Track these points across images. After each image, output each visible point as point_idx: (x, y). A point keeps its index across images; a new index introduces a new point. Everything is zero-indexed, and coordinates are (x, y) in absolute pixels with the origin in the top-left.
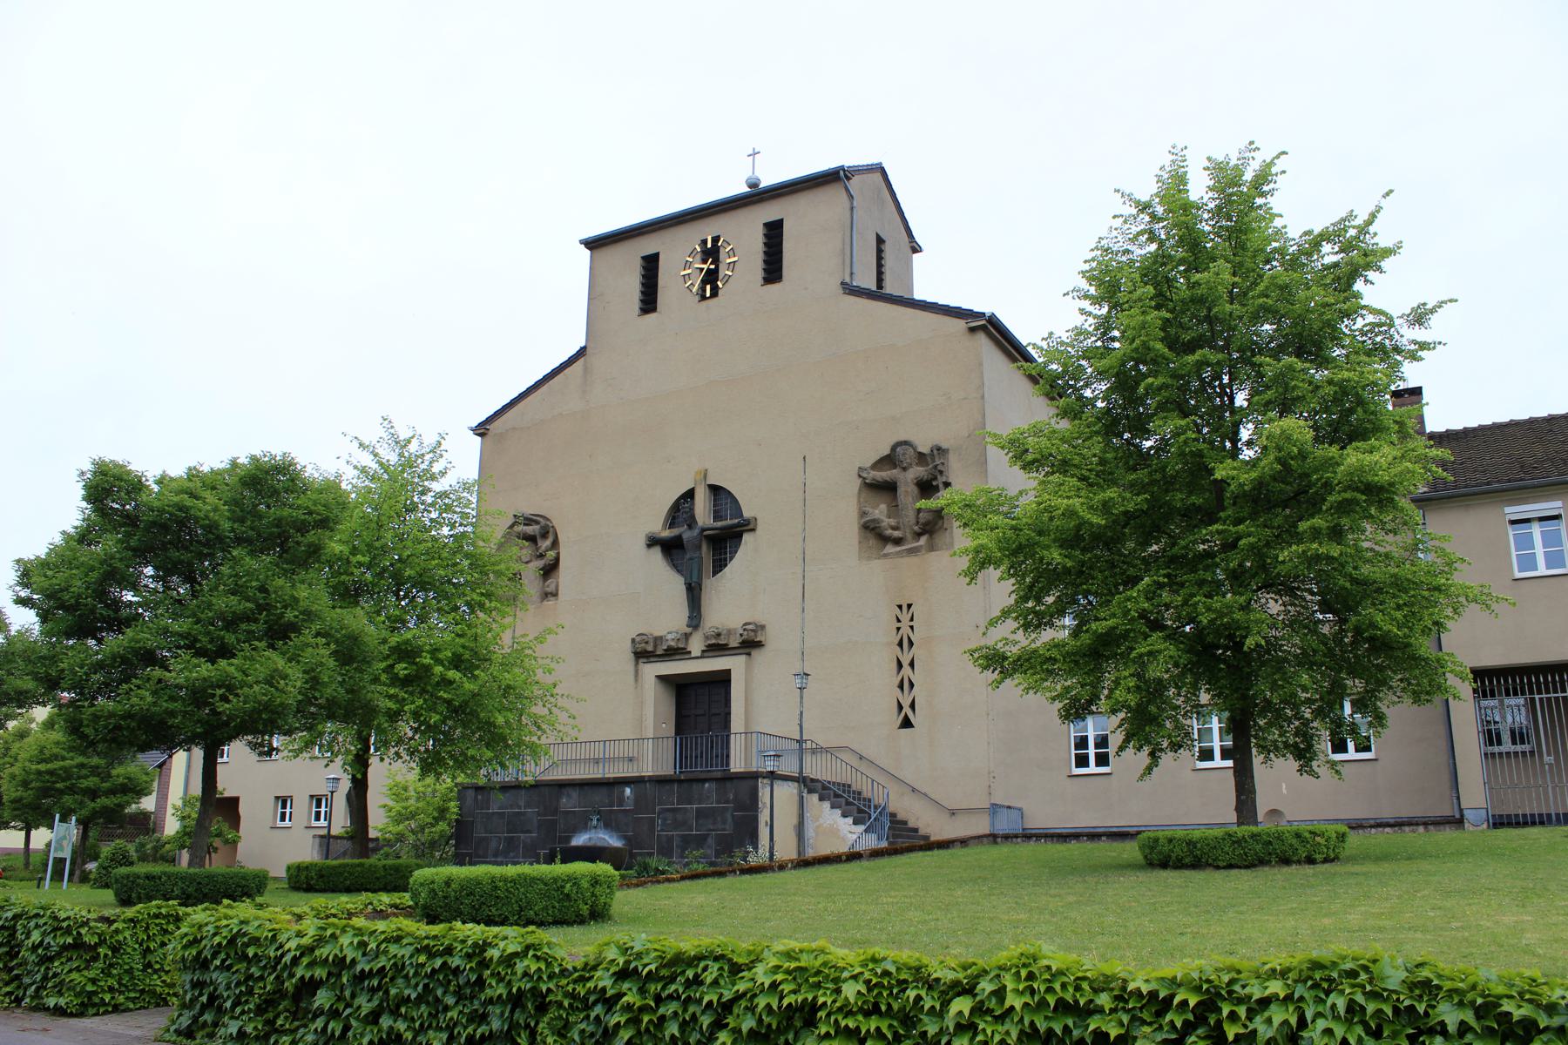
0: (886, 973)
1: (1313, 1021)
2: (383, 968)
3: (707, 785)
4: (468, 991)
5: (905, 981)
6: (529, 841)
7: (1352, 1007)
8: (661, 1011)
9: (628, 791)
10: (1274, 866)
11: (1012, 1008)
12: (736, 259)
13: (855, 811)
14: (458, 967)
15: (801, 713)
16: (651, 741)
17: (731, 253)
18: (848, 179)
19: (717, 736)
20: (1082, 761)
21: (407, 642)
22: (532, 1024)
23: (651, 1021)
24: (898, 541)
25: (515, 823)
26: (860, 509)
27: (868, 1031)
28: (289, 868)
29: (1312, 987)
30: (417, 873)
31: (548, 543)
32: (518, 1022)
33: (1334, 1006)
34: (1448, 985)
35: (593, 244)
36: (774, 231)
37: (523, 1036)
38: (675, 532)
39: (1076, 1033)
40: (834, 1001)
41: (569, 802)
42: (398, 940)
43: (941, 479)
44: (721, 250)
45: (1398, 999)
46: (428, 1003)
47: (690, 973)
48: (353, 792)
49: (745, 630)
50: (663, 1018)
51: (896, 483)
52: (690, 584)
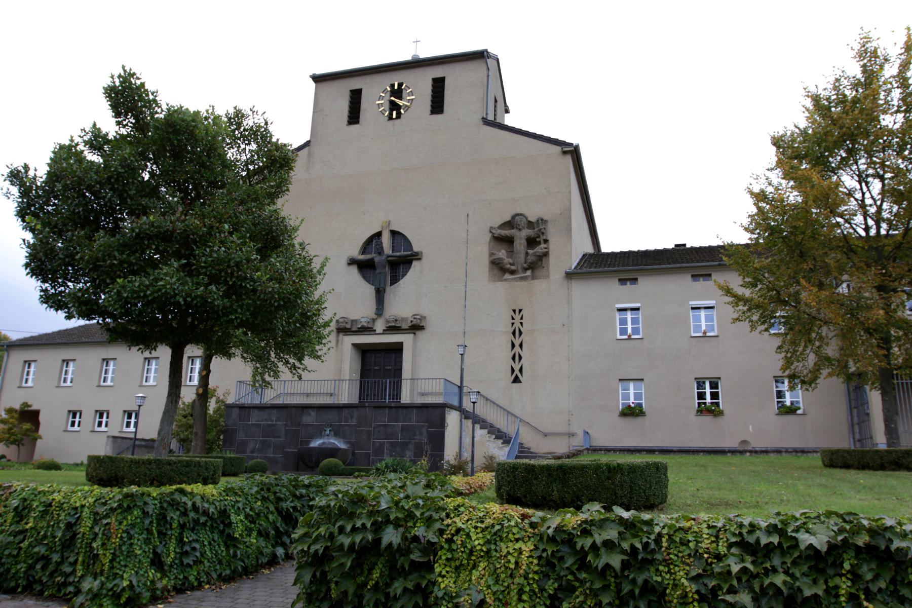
12: (413, 97)
16: (333, 382)
24: (513, 272)
35: (318, 79)
36: (439, 85)
41: (309, 419)
43: (542, 238)
44: (404, 91)
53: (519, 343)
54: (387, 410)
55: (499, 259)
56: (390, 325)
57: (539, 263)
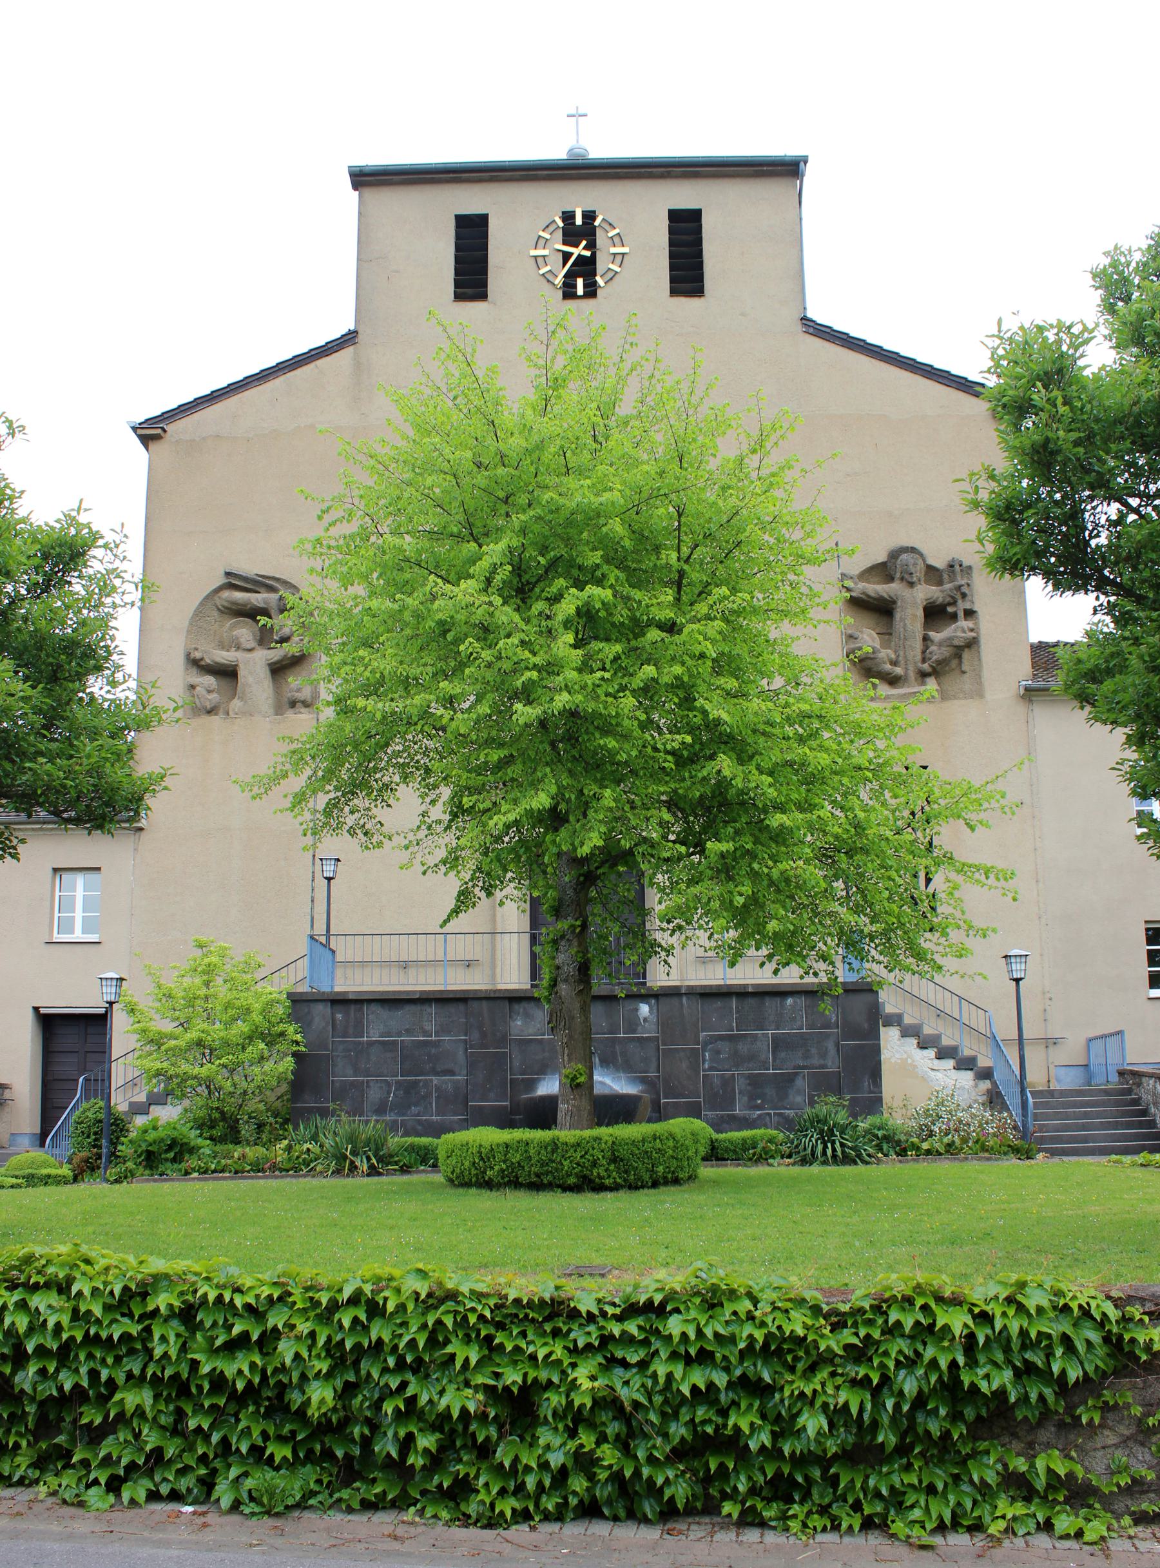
3: (790, 1001)
9: (644, 1009)
12: (625, 250)
24: (893, 681)
35: (362, 179)
43: (962, 605)
51: (894, 602)
54: (734, 1002)
57: (954, 663)
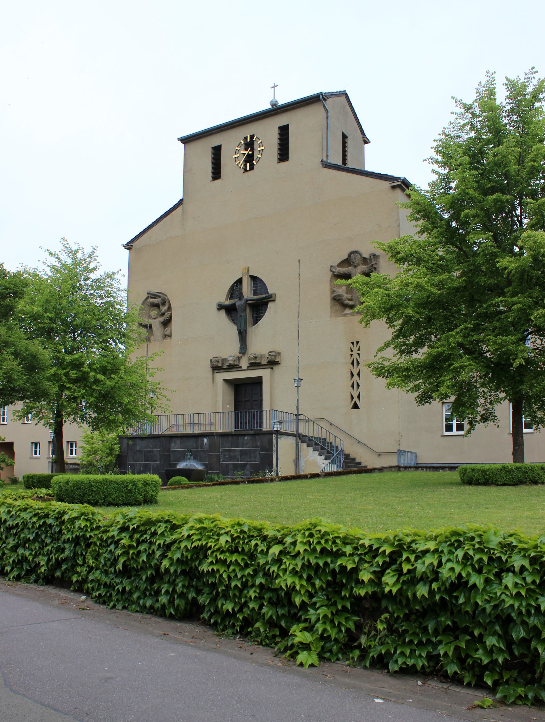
0: (242, 532)
1: (445, 563)
2: (17, 524)
3: (246, 438)
4: (56, 536)
5: (253, 536)
6: (155, 465)
7: (466, 557)
8: (139, 548)
9: (205, 440)
10: (528, 485)
11: (299, 552)
12: (263, 148)
13: (326, 452)
14: (51, 524)
15: (298, 400)
17: (261, 144)
18: (325, 100)
19: (257, 412)
20: (449, 428)
21: (76, 359)
22: (84, 553)
23: (134, 553)
24: (352, 307)
25: (148, 457)
26: (331, 289)
27: (231, 561)
28: (24, 477)
29: (449, 545)
30: (54, 478)
31: (166, 308)
32: (77, 552)
33: (457, 556)
34: (521, 546)
35: (186, 140)
36: (284, 131)
37: (80, 559)
38: (232, 301)
39: (332, 566)
40: (215, 545)
41: (175, 446)
42: (25, 510)
44: (255, 142)
45: (493, 553)
46: (39, 542)
47: (153, 529)
48: (55, 439)
49: (269, 355)
50: (139, 552)
52: (240, 330)
53: (357, 373)
55: (339, 295)
56: (251, 362)
